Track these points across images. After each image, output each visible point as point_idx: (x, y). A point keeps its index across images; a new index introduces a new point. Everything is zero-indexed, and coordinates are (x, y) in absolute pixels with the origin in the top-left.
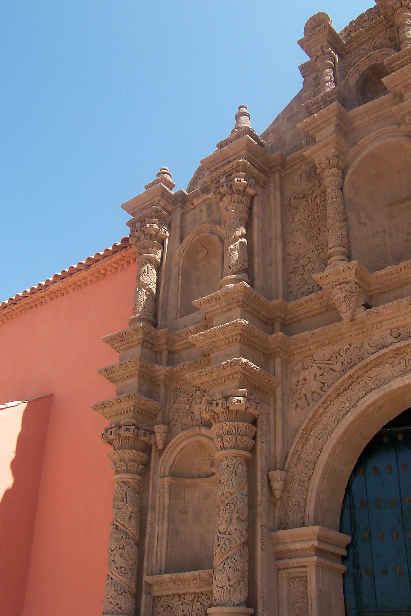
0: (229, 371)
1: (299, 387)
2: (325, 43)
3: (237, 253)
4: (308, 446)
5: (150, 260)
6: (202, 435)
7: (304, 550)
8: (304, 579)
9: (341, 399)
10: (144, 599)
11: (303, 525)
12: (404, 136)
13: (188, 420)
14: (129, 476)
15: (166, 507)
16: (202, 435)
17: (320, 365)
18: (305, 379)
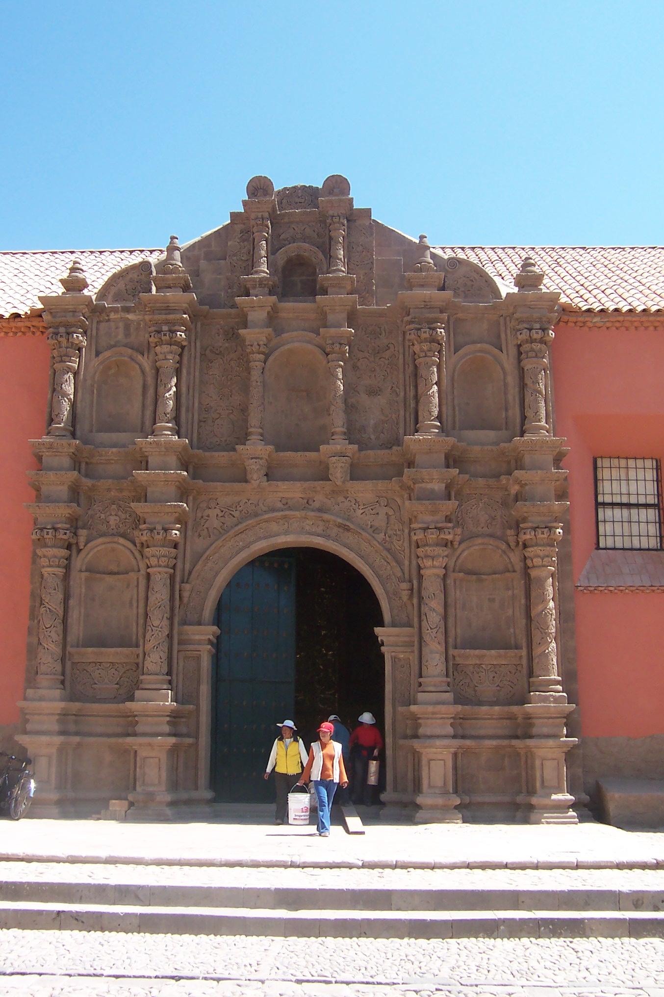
0: (170, 510)
1: (203, 521)
2: (266, 215)
3: (171, 402)
4: (206, 568)
5: (69, 369)
6: (119, 543)
7: (200, 640)
8: (199, 658)
9: (237, 538)
10: (68, 664)
11: (200, 624)
12: (316, 345)
13: (104, 528)
14: (60, 570)
15: (83, 596)
16: (119, 543)
17: (222, 509)
18: (208, 516)
